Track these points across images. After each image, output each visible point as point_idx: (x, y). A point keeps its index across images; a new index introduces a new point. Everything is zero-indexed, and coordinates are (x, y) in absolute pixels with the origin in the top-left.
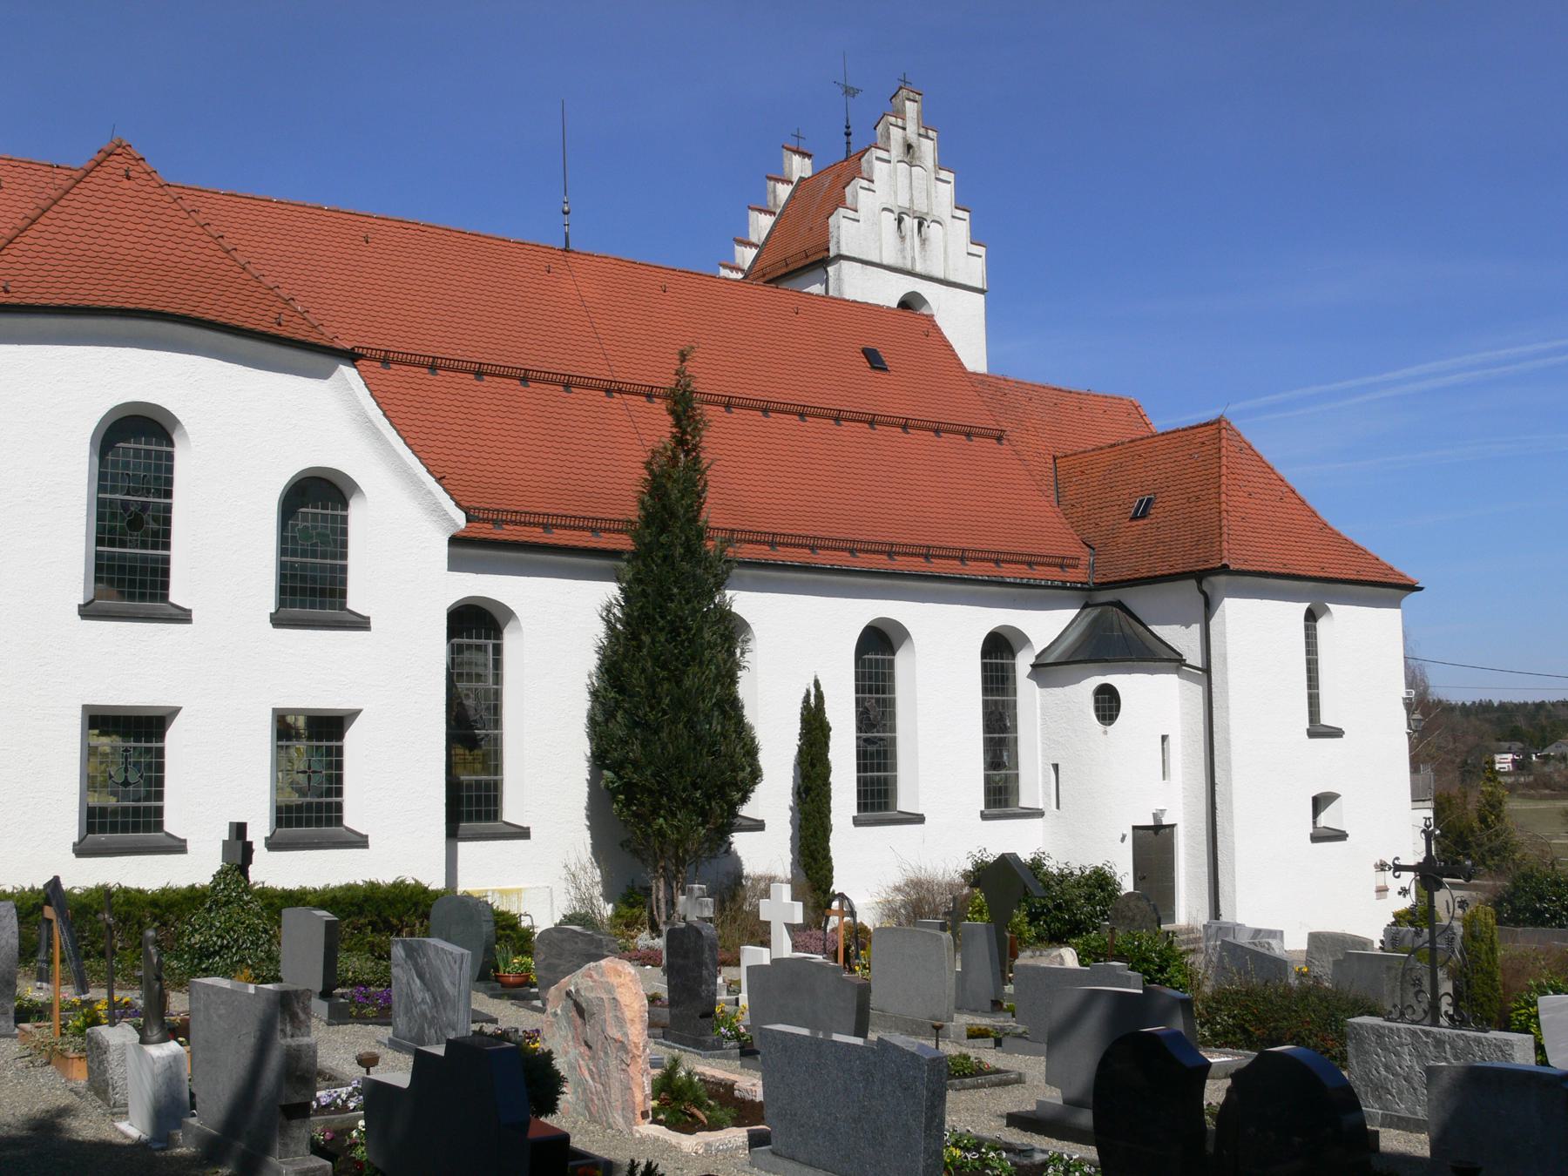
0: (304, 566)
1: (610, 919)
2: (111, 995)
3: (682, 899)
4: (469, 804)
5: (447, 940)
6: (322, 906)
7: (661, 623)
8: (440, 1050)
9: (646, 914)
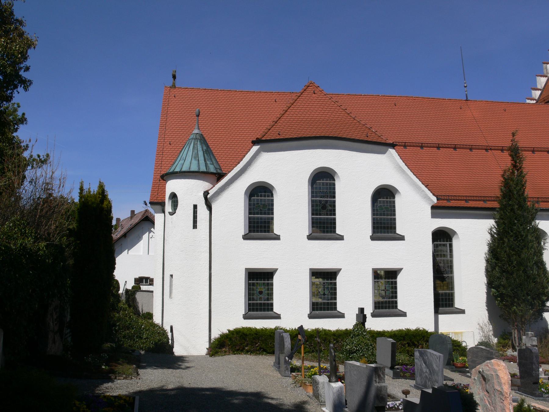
0: (381, 219)
1: (496, 344)
2: (319, 365)
3: (524, 337)
4: (442, 301)
5: (435, 350)
6: (390, 337)
7: (512, 234)
8: (430, 391)
9: (510, 342)
